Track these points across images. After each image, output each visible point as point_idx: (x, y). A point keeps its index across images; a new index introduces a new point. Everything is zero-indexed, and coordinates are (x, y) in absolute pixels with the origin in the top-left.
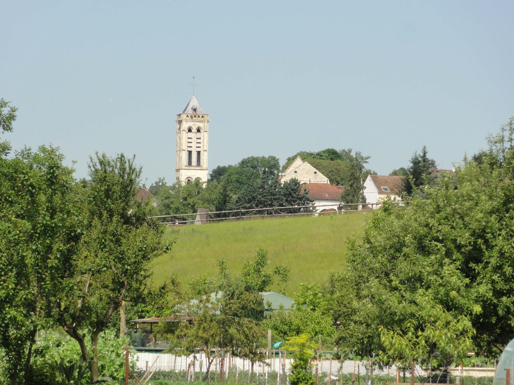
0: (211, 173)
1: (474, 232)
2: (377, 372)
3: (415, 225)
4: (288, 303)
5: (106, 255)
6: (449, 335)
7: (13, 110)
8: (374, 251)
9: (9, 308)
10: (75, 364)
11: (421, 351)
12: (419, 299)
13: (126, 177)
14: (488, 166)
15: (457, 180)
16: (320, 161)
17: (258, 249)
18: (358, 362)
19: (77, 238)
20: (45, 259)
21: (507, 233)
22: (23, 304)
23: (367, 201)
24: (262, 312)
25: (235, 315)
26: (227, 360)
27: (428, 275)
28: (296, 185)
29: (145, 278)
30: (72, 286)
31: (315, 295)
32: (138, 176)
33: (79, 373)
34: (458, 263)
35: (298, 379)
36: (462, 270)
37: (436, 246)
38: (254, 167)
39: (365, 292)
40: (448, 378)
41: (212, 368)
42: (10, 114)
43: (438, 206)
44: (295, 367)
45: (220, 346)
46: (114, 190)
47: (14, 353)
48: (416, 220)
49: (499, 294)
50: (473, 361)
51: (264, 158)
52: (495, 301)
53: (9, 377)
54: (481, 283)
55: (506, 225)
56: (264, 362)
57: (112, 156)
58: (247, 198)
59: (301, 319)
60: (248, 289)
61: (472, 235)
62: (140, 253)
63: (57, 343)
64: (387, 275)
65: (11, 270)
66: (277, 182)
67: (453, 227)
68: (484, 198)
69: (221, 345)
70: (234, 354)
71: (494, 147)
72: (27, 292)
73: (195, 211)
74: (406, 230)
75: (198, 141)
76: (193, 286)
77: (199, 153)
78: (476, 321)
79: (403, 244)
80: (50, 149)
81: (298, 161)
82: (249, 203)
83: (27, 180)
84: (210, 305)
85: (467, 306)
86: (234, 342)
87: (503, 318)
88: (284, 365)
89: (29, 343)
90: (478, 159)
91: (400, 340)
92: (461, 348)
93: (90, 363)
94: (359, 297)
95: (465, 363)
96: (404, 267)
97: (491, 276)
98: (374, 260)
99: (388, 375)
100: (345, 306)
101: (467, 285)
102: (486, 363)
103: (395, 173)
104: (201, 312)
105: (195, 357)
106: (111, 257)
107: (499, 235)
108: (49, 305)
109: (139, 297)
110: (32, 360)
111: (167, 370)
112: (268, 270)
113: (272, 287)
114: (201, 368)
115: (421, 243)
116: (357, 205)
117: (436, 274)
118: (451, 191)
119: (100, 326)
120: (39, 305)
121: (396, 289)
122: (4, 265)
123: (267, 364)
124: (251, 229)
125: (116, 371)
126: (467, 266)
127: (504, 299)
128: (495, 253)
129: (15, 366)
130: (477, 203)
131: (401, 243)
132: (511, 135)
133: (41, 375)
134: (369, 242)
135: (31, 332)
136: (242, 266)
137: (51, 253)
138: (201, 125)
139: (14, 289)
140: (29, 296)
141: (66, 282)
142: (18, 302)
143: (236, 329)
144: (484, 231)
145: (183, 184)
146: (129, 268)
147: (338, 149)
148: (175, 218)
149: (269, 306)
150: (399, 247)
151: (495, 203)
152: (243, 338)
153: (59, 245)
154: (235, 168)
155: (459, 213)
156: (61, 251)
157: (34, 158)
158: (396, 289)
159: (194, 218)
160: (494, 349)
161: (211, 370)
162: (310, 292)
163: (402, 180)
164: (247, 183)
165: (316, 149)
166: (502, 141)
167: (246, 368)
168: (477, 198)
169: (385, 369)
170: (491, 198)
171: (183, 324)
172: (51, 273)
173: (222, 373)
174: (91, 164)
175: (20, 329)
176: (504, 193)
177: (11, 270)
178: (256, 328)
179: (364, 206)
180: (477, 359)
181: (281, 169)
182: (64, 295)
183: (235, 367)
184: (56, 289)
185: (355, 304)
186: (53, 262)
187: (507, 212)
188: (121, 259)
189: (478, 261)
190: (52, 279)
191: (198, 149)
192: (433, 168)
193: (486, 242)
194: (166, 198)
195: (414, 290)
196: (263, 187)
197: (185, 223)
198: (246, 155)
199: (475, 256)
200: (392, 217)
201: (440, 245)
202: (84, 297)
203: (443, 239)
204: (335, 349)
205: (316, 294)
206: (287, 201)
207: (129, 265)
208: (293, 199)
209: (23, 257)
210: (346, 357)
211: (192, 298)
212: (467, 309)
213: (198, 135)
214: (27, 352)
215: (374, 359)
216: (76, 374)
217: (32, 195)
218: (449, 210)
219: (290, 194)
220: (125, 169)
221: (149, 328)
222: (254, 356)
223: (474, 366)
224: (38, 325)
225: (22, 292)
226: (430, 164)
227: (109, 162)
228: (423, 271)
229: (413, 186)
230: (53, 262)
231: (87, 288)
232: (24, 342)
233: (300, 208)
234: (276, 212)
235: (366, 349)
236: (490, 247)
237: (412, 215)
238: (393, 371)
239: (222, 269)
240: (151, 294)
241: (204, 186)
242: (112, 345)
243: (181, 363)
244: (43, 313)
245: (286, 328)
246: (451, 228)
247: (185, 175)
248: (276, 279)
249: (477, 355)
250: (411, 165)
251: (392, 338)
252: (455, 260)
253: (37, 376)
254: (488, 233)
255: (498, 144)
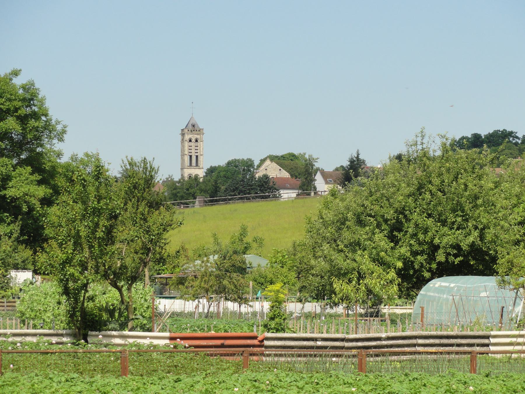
0: (206, 171)
1: (397, 210)
2: (329, 310)
3: (355, 205)
4: (264, 262)
5: (137, 228)
6: (382, 283)
7: (65, 127)
8: (325, 224)
9: (69, 267)
10: (116, 306)
11: (362, 294)
12: (358, 258)
13: (148, 174)
14: (406, 162)
15: (385, 172)
16: (284, 161)
17: (241, 225)
18: (315, 304)
19: (116, 217)
20: (94, 232)
21: (420, 210)
22: (79, 265)
23: (317, 190)
24: (245, 269)
25: (227, 271)
26: (222, 303)
27: (364, 241)
28: (267, 178)
29: (165, 244)
30: (114, 251)
31: (283, 256)
32: (156, 173)
33: (119, 313)
34: (386, 232)
35: (275, 315)
36: (388, 237)
37: (370, 220)
38: (236, 167)
39: (319, 254)
40: (379, 314)
41: (212, 309)
42: (63, 130)
43: (371, 192)
44: (273, 307)
45: (217, 294)
46: (139, 184)
47: (72, 299)
48: (355, 202)
49: (415, 254)
50: (396, 302)
51: (243, 159)
52: (412, 259)
53: (69, 317)
54: (402, 246)
55: (420, 204)
56: (248, 305)
57: (138, 159)
58: (232, 188)
59: (273, 274)
60: (235, 252)
61: (395, 212)
62: (162, 227)
63: (103, 292)
64: (335, 241)
65: (70, 240)
66: (253, 177)
67: (381, 207)
68: (403, 185)
69: (217, 292)
70: (226, 299)
71: (410, 149)
72: (81, 255)
73: (195, 198)
74: (348, 209)
75: (196, 148)
76: (195, 251)
77: (197, 156)
78: (399, 273)
79: (346, 219)
80: (91, 154)
81: (268, 162)
82: (234, 192)
83: (80, 176)
84: (209, 265)
85: (393, 262)
86: (227, 290)
87: (418, 270)
88: (262, 306)
89: (83, 291)
90: (399, 157)
91: (347, 287)
92: (390, 292)
93: (127, 306)
94: (315, 257)
95: (391, 304)
96: (346, 235)
97: (409, 241)
98: (326, 231)
99: (336, 313)
100: (306, 264)
101: (392, 247)
102: (406, 303)
103: (337, 169)
104: (203, 269)
105: (199, 301)
106: (141, 230)
107: (415, 212)
108: (97, 265)
109: (161, 258)
110: (85, 304)
111: (179, 311)
112: (248, 239)
113: (252, 251)
114: (204, 309)
115: (359, 218)
116: (310, 193)
117: (370, 240)
118: (380, 180)
119: (134, 278)
120: (90, 265)
121: (342, 251)
122: (64, 237)
123: (250, 306)
124: (236, 210)
125: (145, 312)
126: (392, 234)
127: (419, 257)
128: (412, 225)
129: (74, 308)
130: (398, 189)
131: (345, 218)
132: (422, 140)
133: (92, 315)
134: (322, 218)
135: (85, 284)
136: (230, 237)
137: (99, 228)
138: (198, 137)
139: (72, 254)
140: (83, 259)
141: (109, 248)
142: (75, 263)
143: (228, 281)
144: (404, 209)
145: (186, 179)
146: (154, 238)
147: (296, 153)
148: (181, 203)
149: (250, 265)
150: (343, 221)
151: (412, 189)
152: (233, 288)
153: (104, 222)
154: (222, 167)
155: (386, 197)
156: (105, 226)
157: (81, 161)
158: (342, 251)
159: (194, 203)
160: (412, 293)
161: (210, 310)
162: (280, 254)
163: (342, 174)
164: (231, 178)
165: (280, 153)
166: (416, 144)
167: (235, 309)
168: (398, 185)
169: (334, 308)
170: (408, 185)
171: (190, 278)
172: (99, 242)
173: (218, 313)
174: (123, 165)
175: (77, 282)
176: (418, 182)
177: (70, 240)
178: (242, 280)
179: (315, 193)
180: (399, 300)
181: (255, 167)
182: (108, 258)
183: (227, 308)
184: (102, 253)
185: (313, 262)
186: (100, 234)
187: (420, 196)
188: (148, 232)
189: (400, 230)
190: (100, 246)
191: (196, 154)
192: (364, 166)
193: (405, 216)
194: (174, 189)
195: (354, 251)
196: (243, 181)
197: (188, 207)
198: (231, 158)
199: (398, 227)
200: (338, 200)
201: (372, 219)
202: (122, 259)
203: (375, 215)
204: (298, 294)
205: (284, 256)
206: (260, 190)
207: (154, 236)
208: (265, 189)
209: (78, 231)
210: (306, 301)
211: (197, 260)
212: (392, 265)
213: (196, 144)
214: (82, 299)
215: (326, 301)
216: (117, 315)
217: (84, 186)
218: (378, 194)
219: (263, 185)
220: (147, 168)
221: (165, 282)
222: (241, 300)
223: (397, 305)
224: (89, 279)
225: (78, 255)
226: (361, 163)
227: (135, 164)
228: (361, 238)
229: (353, 178)
230: (100, 234)
231: (123, 252)
232: (79, 292)
233: (270, 195)
234: (253, 198)
235: (323, 293)
236: (408, 220)
237: (351, 199)
238: (340, 309)
239: (215, 239)
240: (169, 256)
241: (201, 180)
242: (142, 294)
243: (189, 306)
244: (93, 271)
245: (263, 280)
246: (380, 207)
247: (187, 172)
248: (254, 245)
249: (400, 297)
250: (349, 163)
251: (342, 285)
252: (383, 230)
253: (89, 316)
254: (407, 211)
255: (413, 147)
